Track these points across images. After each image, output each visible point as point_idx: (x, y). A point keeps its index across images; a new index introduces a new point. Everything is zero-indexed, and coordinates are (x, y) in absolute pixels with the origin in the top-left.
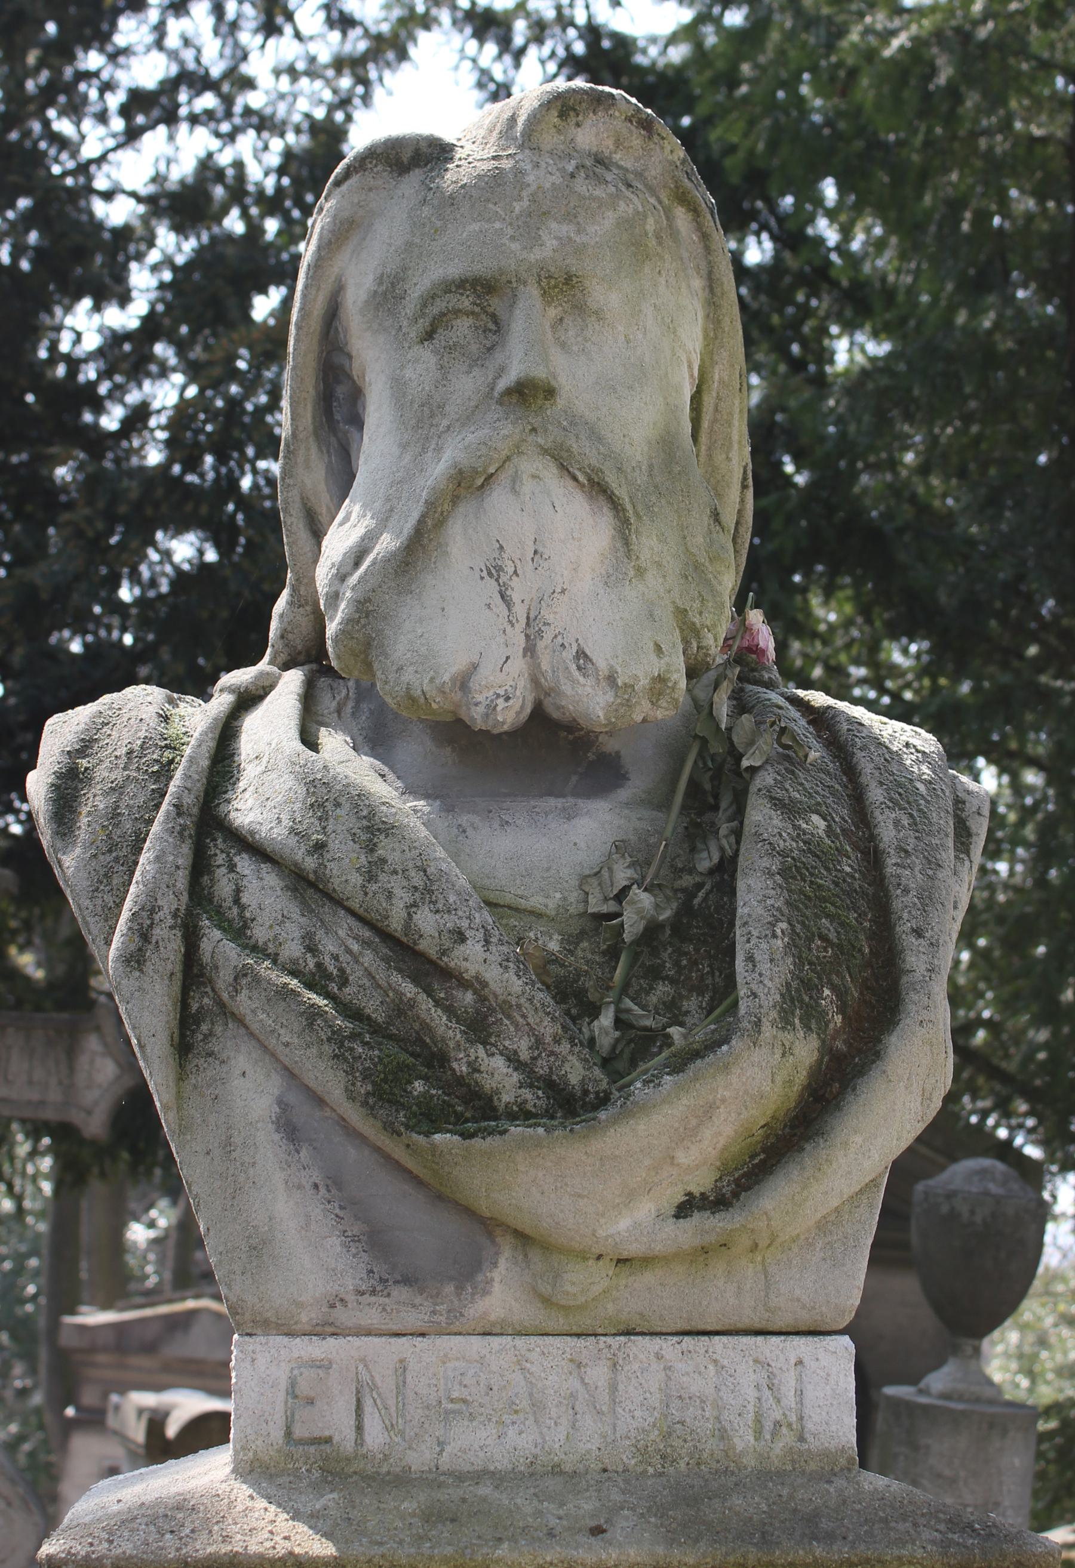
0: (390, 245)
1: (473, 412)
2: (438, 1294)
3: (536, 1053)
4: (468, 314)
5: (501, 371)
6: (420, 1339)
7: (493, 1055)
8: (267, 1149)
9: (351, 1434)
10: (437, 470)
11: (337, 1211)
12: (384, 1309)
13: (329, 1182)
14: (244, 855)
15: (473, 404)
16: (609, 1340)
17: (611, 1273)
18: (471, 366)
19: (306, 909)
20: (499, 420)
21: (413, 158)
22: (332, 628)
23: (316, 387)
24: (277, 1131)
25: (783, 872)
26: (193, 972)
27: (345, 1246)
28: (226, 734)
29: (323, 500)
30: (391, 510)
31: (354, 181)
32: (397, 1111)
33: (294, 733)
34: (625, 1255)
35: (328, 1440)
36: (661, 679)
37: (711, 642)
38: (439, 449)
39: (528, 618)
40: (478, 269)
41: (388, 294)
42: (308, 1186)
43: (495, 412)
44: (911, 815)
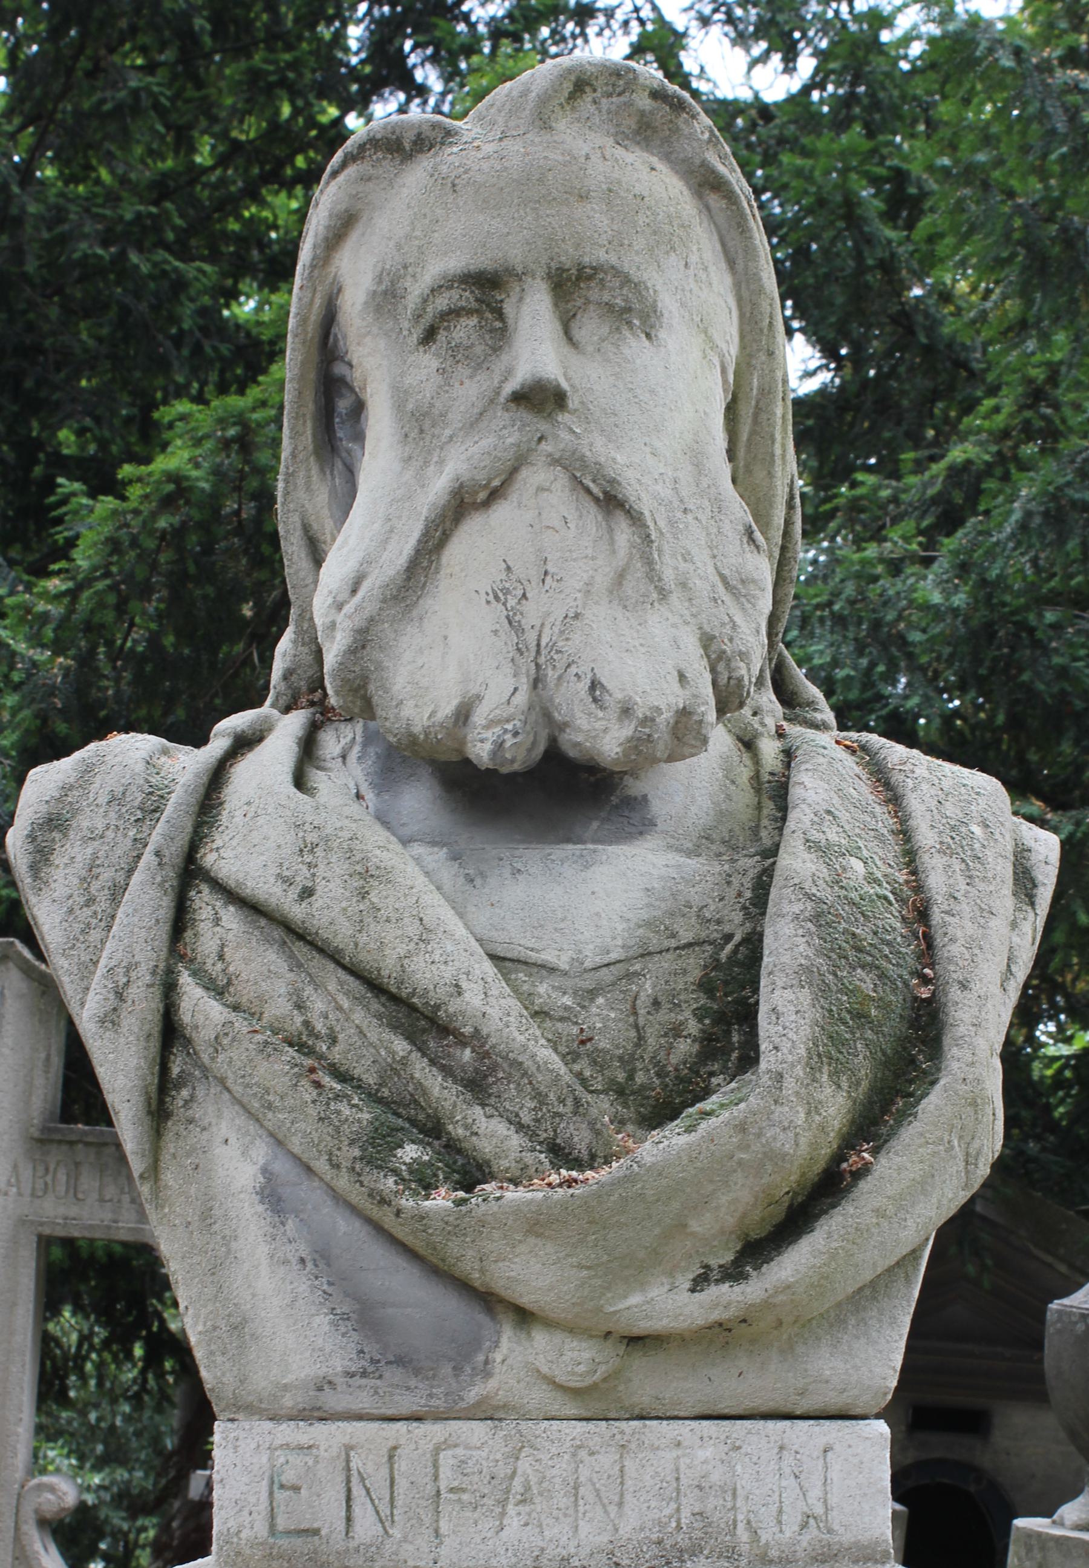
0: (390, 239)
1: (477, 420)
2: (434, 1376)
3: (540, 1114)
4: (470, 312)
5: (509, 373)
6: (415, 1424)
7: (492, 1116)
8: (248, 1217)
9: (341, 1525)
10: (438, 487)
11: (325, 1287)
12: (376, 1393)
13: (317, 1256)
14: (232, 908)
15: (476, 410)
16: (623, 1425)
17: (621, 1353)
18: (476, 369)
19: (297, 965)
20: (504, 427)
21: (415, 143)
22: (330, 660)
23: (316, 402)
24: (262, 1202)
25: (817, 918)
26: (170, 1032)
27: (334, 1324)
28: (217, 777)
29: (324, 523)
30: (391, 531)
31: (352, 170)
32: (385, 1176)
33: (288, 778)
34: (636, 1332)
35: (316, 1532)
36: (684, 713)
37: (744, 672)
38: (441, 462)
39: (538, 645)
40: (482, 262)
41: (387, 297)
42: (294, 1261)
43: (501, 417)
44: (963, 861)
